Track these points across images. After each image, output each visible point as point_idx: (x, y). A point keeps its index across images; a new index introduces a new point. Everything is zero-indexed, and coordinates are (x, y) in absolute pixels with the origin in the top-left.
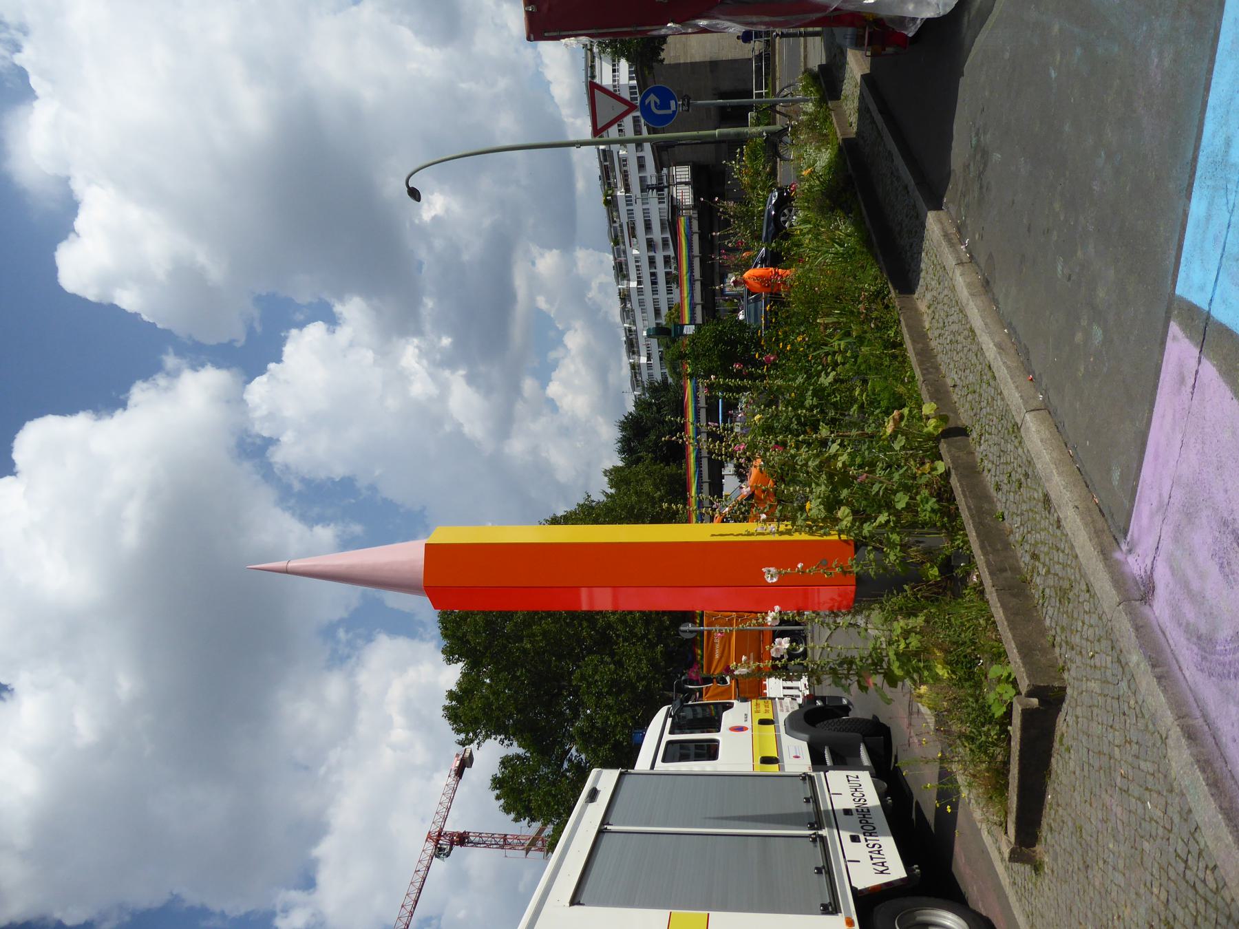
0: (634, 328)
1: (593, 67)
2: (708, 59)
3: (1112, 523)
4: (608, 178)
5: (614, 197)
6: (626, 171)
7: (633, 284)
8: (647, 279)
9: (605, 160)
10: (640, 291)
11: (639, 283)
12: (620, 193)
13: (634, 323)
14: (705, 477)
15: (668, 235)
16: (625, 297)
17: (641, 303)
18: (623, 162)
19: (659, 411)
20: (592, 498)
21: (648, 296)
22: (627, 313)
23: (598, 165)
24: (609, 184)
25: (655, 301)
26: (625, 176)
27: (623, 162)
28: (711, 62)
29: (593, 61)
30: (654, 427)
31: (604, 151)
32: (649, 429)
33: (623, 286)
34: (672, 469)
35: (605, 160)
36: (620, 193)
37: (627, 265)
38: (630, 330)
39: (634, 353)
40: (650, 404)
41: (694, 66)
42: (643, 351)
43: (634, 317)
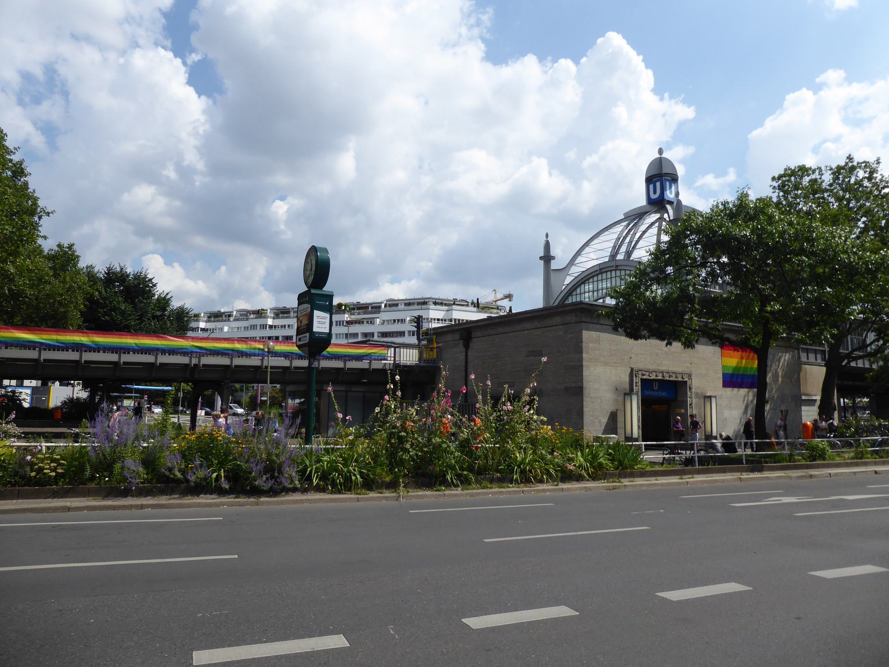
0: (231, 319)
1: (442, 304)
2: (585, 384)
3: (181, 322)
4: (358, 308)
5: (344, 312)
6: (363, 322)
7: (270, 322)
8: (273, 333)
9: (372, 308)
10: (264, 327)
11: (271, 327)
12: (346, 317)
13: (236, 320)
14: (47, 355)
15: (360, 339)
16: (260, 313)
17: (254, 327)
18: (371, 322)
19: (154, 317)
20: (45, 218)
21: (258, 333)
22: (245, 315)
23: (368, 302)
24: (354, 309)
25: (254, 339)
26: (359, 322)
27: (371, 322)
28: (582, 387)
29: (446, 305)
30: (135, 307)
31: (380, 307)
32: (133, 302)
33: (269, 314)
34: (75, 316)
35: (372, 308)
36: (346, 317)
37: (287, 317)
38: (230, 316)
39: (209, 317)
40: (164, 310)
41: (577, 369)
42: (210, 325)
43: (241, 320)
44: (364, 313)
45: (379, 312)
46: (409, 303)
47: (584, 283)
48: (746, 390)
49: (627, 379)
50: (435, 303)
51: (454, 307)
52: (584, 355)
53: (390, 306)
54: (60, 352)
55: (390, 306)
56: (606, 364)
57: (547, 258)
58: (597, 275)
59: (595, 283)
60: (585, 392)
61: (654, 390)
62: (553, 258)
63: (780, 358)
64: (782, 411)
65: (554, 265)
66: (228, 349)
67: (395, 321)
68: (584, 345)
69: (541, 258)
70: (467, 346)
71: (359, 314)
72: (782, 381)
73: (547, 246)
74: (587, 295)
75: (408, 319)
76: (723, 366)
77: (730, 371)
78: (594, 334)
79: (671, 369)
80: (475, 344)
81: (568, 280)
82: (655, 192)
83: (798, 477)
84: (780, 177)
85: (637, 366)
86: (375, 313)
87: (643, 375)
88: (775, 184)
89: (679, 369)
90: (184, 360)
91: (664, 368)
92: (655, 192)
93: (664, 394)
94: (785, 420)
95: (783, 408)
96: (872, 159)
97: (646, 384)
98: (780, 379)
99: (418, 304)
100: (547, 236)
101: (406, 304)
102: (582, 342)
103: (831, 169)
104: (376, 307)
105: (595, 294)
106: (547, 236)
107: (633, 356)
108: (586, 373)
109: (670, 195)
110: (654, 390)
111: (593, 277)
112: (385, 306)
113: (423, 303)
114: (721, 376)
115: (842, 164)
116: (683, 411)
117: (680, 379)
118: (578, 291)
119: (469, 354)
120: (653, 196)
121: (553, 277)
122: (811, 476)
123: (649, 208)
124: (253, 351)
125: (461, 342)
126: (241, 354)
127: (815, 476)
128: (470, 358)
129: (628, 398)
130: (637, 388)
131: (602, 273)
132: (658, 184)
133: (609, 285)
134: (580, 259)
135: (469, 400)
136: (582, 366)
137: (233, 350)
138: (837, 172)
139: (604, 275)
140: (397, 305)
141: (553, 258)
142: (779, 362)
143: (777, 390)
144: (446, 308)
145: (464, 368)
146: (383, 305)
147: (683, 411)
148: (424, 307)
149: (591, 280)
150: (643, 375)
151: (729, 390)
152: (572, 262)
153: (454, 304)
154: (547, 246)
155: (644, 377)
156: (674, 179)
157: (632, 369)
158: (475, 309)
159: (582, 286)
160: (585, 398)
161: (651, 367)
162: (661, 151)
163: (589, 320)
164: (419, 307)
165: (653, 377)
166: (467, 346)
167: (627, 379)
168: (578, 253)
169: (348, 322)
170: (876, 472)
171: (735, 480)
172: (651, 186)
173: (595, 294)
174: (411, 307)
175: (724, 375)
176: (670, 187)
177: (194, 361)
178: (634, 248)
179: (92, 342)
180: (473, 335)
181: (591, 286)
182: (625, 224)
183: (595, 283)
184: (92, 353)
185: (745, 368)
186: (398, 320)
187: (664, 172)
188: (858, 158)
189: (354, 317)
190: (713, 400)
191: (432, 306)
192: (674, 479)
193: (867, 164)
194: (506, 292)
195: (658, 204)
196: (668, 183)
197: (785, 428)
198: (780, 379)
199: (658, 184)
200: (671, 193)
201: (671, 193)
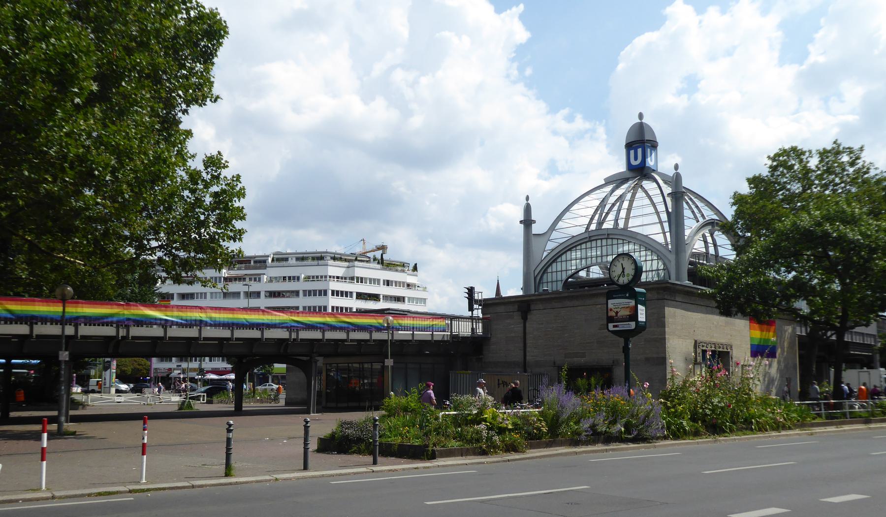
1: (341, 259)
9: (255, 262)
18: (257, 278)
27: (257, 278)
29: (346, 260)
31: (265, 262)
35: (255, 262)
44: (246, 269)
45: (266, 267)
46: (302, 258)
47: (570, 250)
49: (692, 349)
50: (334, 259)
51: (356, 263)
53: (278, 260)
54: (105, 327)
55: (278, 260)
56: (680, 337)
57: (527, 222)
58: (586, 242)
59: (584, 251)
62: (534, 222)
65: (536, 229)
66: (320, 323)
67: (284, 278)
69: (521, 222)
70: (525, 319)
71: (239, 269)
73: (528, 209)
74: (574, 262)
75: (303, 276)
78: (679, 312)
81: (550, 246)
82: (636, 159)
85: (699, 338)
86: (259, 268)
89: (723, 341)
90: (110, 331)
91: (714, 340)
92: (636, 159)
96: (856, 147)
99: (313, 259)
100: (527, 198)
101: (297, 259)
104: (260, 262)
105: (584, 261)
106: (527, 198)
108: (668, 345)
109: (650, 162)
111: (581, 244)
112: (273, 260)
113: (319, 258)
114: (749, 346)
115: (829, 148)
118: (564, 257)
119: (527, 325)
120: (634, 163)
121: (534, 241)
123: (629, 175)
124: (340, 324)
126: (333, 328)
128: (528, 329)
131: (591, 241)
132: (640, 151)
133: (599, 253)
134: (561, 224)
136: (665, 339)
137: (324, 324)
138: (823, 154)
139: (594, 243)
140: (286, 259)
141: (534, 222)
144: (347, 264)
146: (270, 260)
148: (321, 262)
149: (579, 247)
152: (553, 227)
153: (356, 260)
154: (528, 209)
156: (654, 145)
157: (696, 341)
158: (379, 266)
159: (568, 253)
161: (707, 339)
163: (669, 298)
164: (316, 262)
166: (525, 319)
168: (559, 218)
169: (226, 279)
172: (632, 152)
173: (584, 261)
174: (305, 263)
175: (752, 346)
177: (122, 332)
178: (597, 210)
179: (211, 318)
180: (532, 307)
181: (579, 253)
182: (609, 188)
183: (584, 251)
184: (242, 331)
186: (290, 278)
187: (647, 138)
188: (845, 144)
189: (234, 273)
191: (331, 262)
193: (850, 151)
194: (379, 244)
195: (640, 172)
197: (789, 392)
199: (640, 151)
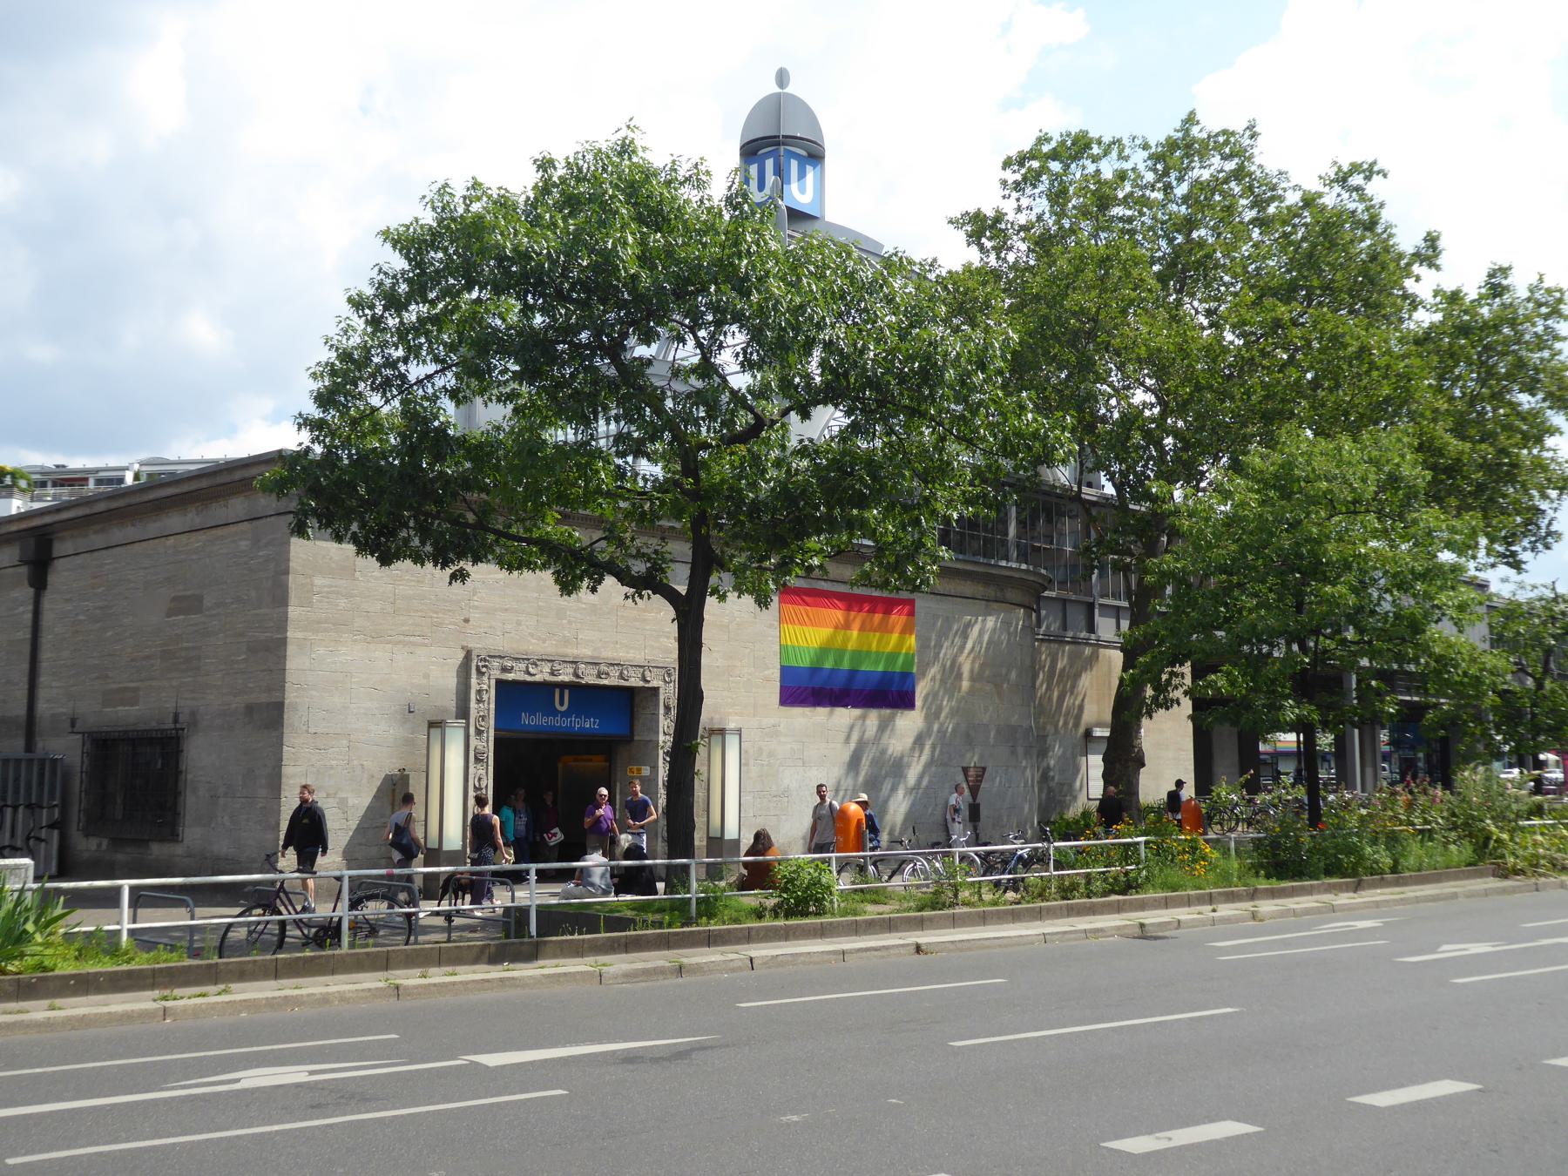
2: (291, 696)
9: (99, 482)
24: (43, 484)
28: (279, 707)
35: (99, 482)
48: (857, 712)
52: (294, 612)
60: (288, 716)
61: (555, 713)
63: (969, 625)
64: (965, 770)
68: (293, 581)
70: (39, 582)
72: (971, 691)
76: (783, 649)
77: (805, 662)
79: (608, 654)
80: (61, 576)
83: (629, 976)
84: (1022, 159)
87: (504, 670)
88: (1012, 176)
91: (585, 652)
93: (590, 724)
94: (974, 791)
95: (973, 760)
97: (512, 695)
98: (965, 684)
102: (287, 572)
103: (1146, 147)
107: (475, 616)
108: (296, 663)
110: (555, 713)
114: (776, 674)
116: (646, 771)
117: (635, 682)
119: (46, 604)
122: (680, 970)
125: (24, 570)
127: (697, 969)
128: (47, 618)
129: (435, 733)
130: (484, 708)
135: (40, 745)
136: (283, 642)
142: (965, 637)
143: (954, 713)
145: (27, 649)
147: (646, 771)
150: (504, 670)
151: (797, 711)
155: (510, 676)
160: (288, 738)
161: (535, 647)
162: (782, 77)
165: (541, 674)
167: (451, 682)
170: (918, 949)
171: (375, 993)
175: (785, 671)
176: (802, 175)
180: (59, 548)
185: (858, 655)
188: (1210, 123)
190: (732, 743)
192: (142, 1002)
196: (794, 164)
197: (974, 813)
198: (965, 684)
199: (769, 163)
200: (802, 190)
201: (802, 190)
